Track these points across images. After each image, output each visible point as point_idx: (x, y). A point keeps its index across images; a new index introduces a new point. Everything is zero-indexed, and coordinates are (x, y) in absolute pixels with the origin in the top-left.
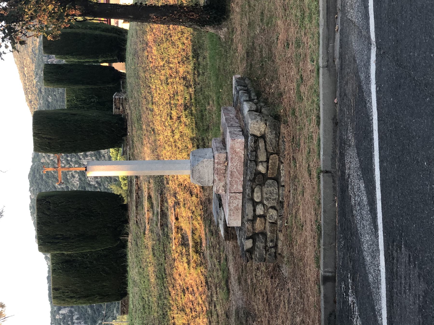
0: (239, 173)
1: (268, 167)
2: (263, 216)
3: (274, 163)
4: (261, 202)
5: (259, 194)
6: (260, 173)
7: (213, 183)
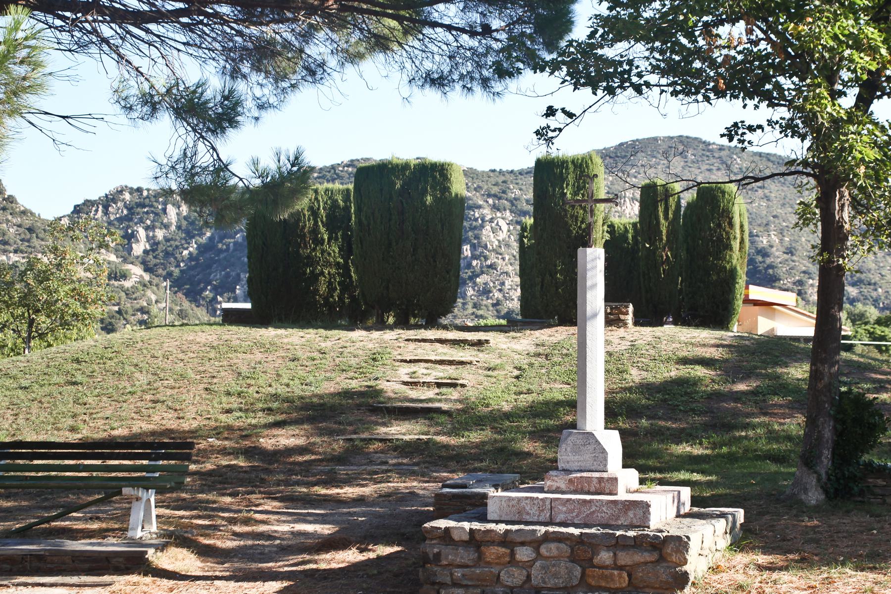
0: (587, 516)
1: (606, 567)
2: (513, 561)
3: (613, 580)
4: (539, 555)
5: (555, 552)
6: (595, 553)
7: (564, 470)
